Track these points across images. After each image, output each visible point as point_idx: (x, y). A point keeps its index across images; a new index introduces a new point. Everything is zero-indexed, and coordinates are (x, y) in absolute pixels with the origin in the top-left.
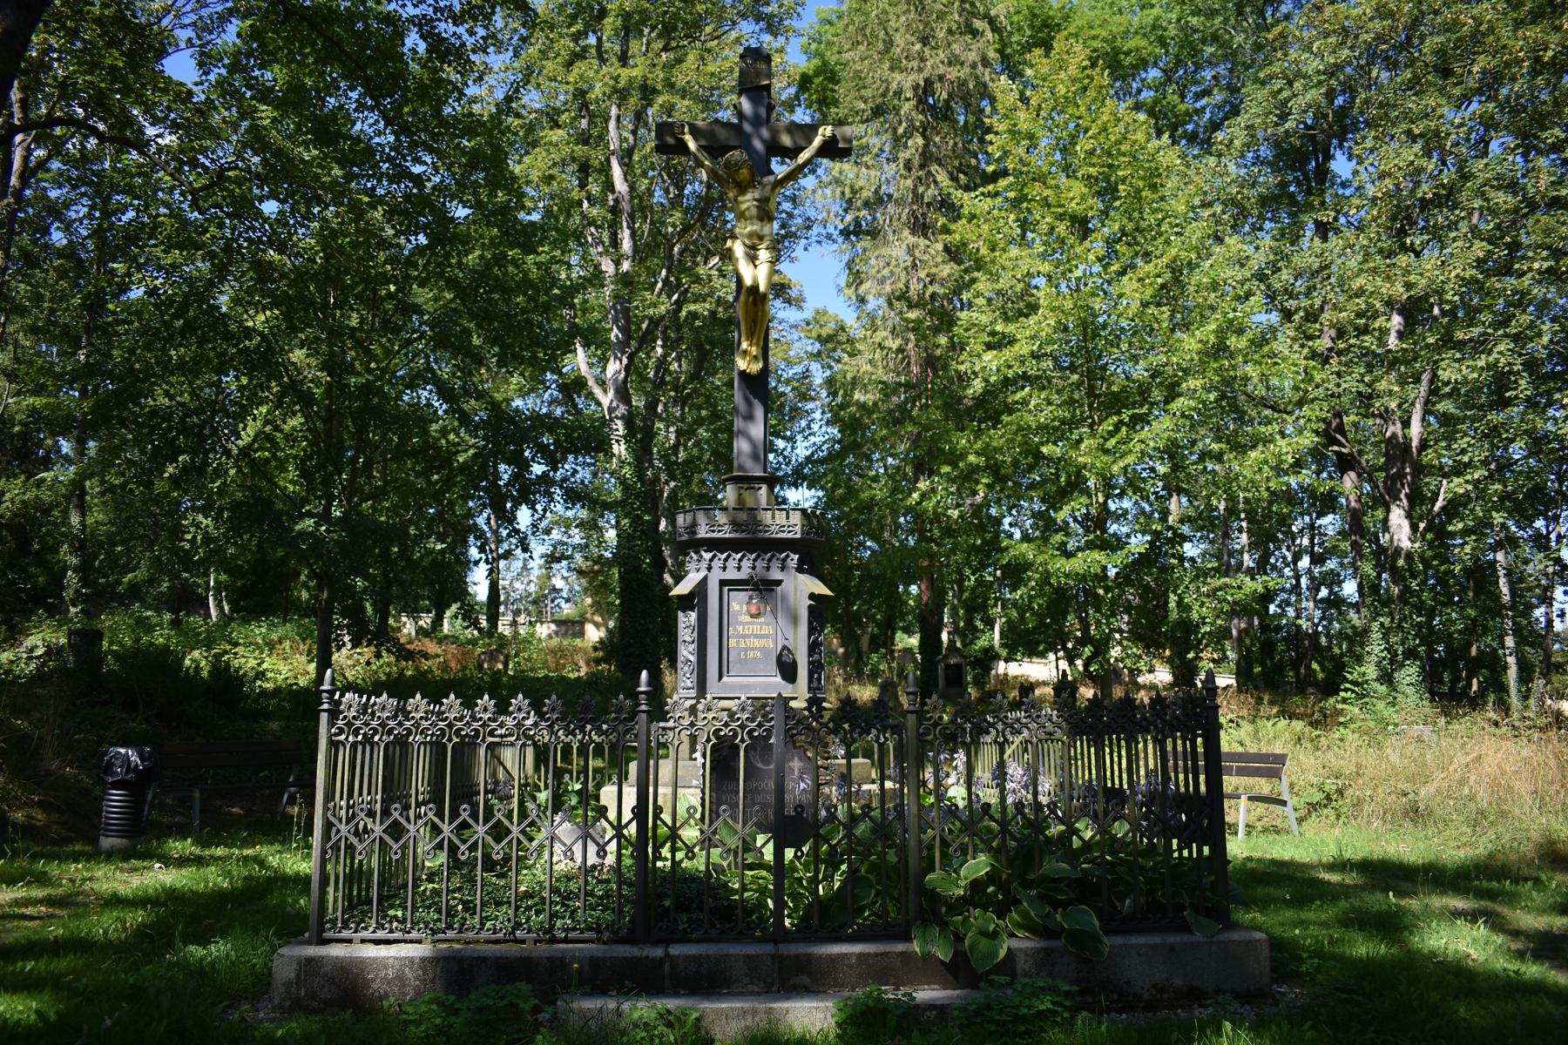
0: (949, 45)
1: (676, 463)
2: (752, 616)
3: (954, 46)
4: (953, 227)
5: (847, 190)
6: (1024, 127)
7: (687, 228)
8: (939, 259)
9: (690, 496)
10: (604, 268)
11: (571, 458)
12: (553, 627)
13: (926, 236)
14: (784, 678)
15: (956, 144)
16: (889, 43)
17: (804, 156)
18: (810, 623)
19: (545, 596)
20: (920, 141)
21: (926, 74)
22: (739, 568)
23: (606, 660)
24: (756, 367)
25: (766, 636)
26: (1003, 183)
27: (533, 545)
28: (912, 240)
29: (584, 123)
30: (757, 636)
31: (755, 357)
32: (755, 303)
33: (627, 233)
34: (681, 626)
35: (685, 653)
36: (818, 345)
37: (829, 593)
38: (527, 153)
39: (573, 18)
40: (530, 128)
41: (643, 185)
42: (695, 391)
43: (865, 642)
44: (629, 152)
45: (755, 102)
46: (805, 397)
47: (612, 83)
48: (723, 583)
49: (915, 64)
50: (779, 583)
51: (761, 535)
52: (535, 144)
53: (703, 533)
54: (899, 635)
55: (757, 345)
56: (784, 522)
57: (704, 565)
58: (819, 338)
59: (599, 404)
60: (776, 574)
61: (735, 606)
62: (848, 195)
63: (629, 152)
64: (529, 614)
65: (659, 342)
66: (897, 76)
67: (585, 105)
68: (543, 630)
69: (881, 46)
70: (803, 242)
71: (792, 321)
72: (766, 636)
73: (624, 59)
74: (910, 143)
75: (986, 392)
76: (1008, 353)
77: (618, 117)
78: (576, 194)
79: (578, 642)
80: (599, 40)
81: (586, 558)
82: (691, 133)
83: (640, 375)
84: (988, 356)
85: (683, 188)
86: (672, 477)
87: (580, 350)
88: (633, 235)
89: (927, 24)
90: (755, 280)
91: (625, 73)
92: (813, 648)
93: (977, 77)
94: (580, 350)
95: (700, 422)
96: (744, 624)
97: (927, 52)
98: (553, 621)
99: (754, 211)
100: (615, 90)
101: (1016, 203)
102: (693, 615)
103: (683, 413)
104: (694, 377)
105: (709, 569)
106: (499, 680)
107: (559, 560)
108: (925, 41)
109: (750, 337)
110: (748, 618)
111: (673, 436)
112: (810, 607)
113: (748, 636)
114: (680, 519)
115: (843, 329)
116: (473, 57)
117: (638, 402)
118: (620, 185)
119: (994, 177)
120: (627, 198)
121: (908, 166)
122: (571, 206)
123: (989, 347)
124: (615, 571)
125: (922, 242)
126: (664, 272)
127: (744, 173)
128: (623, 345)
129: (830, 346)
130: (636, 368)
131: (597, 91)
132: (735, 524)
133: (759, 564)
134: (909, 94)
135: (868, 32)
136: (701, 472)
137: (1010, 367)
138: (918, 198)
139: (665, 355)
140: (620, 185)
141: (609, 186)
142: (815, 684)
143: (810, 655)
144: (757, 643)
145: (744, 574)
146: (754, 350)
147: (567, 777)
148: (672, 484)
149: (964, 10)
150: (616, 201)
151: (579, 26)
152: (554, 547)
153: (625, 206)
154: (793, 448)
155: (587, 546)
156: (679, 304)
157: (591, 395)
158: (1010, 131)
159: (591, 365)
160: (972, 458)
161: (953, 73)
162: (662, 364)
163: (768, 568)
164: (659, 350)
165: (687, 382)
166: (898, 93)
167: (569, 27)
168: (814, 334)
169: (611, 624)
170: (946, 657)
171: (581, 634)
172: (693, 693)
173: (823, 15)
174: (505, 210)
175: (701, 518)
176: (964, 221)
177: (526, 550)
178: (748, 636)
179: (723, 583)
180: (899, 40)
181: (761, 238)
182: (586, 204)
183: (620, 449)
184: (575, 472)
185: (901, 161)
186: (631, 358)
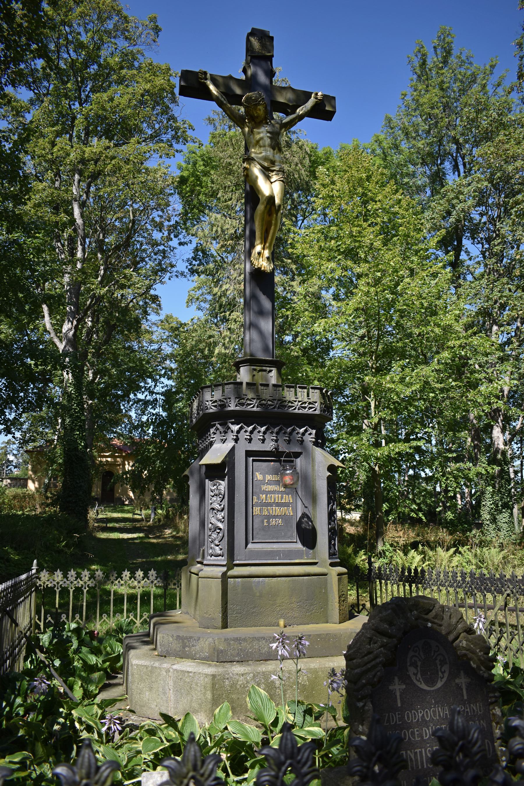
5: (219, 229)
12: (9, 481)
14: (304, 544)
17: (300, 111)
30: (278, 505)
32: (270, 214)
33: (80, 248)
35: (213, 520)
48: (249, 454)
56: (306, 400)
61: (259, 476)
70: (168, 274)
71: (153, 321)
99: (268, 141)
102: (223, 485)
105: (236, 440)
112: (329, 478)
120: (81, 227)
143: (329, 524)
144: (277, 511)
145: (269, 446)
147: (64, 617)
154: (155, 386)
171: (25, 486)
172: (223, 561)
186: (78, 321)
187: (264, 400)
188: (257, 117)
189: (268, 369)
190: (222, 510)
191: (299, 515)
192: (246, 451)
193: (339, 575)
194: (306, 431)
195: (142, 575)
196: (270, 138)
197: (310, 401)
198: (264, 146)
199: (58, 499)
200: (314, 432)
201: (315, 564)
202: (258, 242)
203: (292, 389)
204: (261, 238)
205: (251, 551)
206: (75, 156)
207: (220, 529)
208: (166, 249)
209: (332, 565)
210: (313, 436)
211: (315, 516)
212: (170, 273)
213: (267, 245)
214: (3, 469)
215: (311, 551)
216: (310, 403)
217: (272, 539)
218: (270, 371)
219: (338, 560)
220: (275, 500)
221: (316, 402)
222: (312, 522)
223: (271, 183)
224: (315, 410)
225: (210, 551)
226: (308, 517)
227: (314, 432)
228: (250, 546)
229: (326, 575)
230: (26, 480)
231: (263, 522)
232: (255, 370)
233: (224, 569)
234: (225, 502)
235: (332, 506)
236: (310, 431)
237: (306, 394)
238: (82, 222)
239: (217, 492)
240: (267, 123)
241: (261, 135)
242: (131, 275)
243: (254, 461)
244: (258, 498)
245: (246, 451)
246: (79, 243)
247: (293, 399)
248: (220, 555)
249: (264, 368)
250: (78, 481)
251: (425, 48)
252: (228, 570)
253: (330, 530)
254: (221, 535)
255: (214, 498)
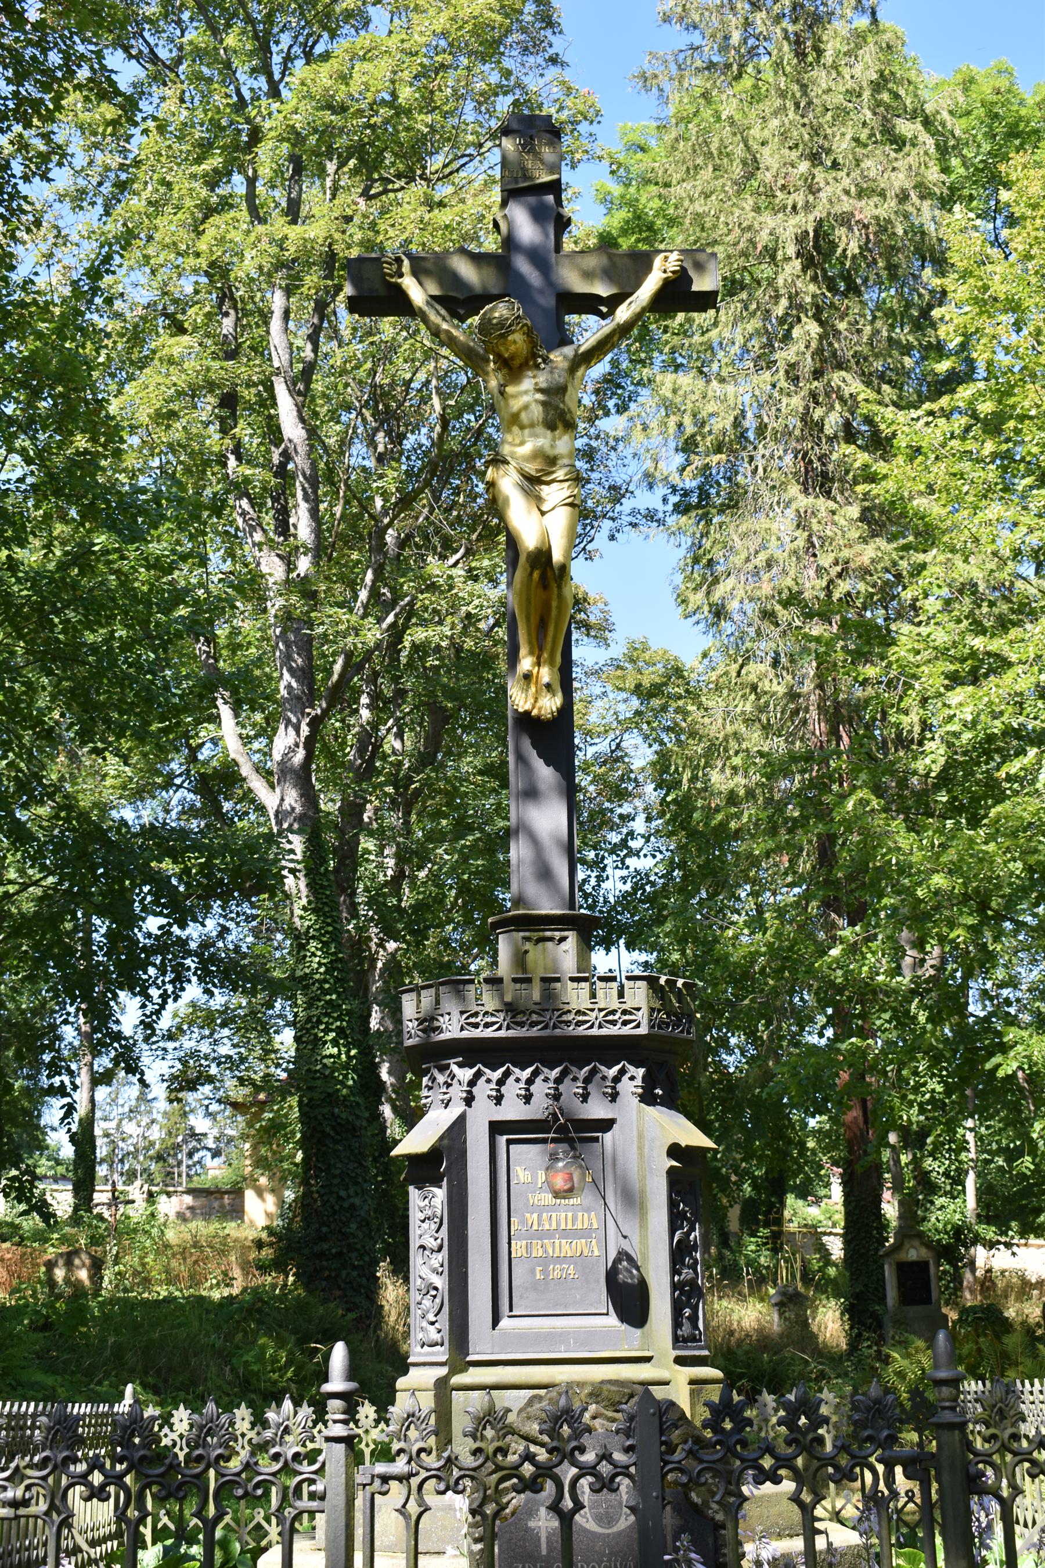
0: (858, 162)
1: (398, 908)
2: (557, 1195)
3: (867, 164)
4: (880, 467)
5: (687, 420)
6: (999, 289)
7: (406, 501)
8: (854, 534)
9: (423, 968)
10: (264, 569)
11: (216, 906)
12: (188, 1200)
13: (828, 495)
14: (623, 1317)
15: (876, 332)
16: (752, 166)
17: (623, 313)
18: (672, 1204)
19: (178, 1147)
20: (814, 328)
21: (819, 213)
22: (528, 1098)
23: (278, 1265)
24: (550, 704)
25: (585, 1234)
26: (965, 393)
27: (146, 1060)
28: (804, 502)
29: (228, 324)
30: (565, 1234)
31: (548, 686)
32: (544, 583)
33: (303, 507)
34: (415, 1216)
35: (425, 1271)
36: (635, 703)
37: (706, 1142)
38: (131, 378)
39: (205, 148)
40: (136, 336)
41: (331, 433)
42: (427, 783)
43: (734, 1224)
44: (309, 370)
45: (538, 215)
46: (621, 795)
47: (274, 250)
48: (496, 1128)
49: (799, 198)
50: (607, 1125)
51: (571, 1030)
52: (143, 364)
53: (451, 1028)
54: (790, 1199)
55: (551, 663)
56: (615, 1004)
57: (457, 1092)
58: (638, 690)
59: (261, 809)
60: (596, 1109)
61: (521, 1174)
62: (690, 429)
63: (309, 370)
64: (150, 1181)
65: (364, 700)
66: (769, 221)
67: (226, 295)
68: (168, 1206)
69: (737, 170)
70: (607, 525)
72: (585, 1234)
73: (293, 212)
74: (796, 332)
75: (950, 765)
76: (996, 688)
77: (286, 315)
78: (214, 441)
79: (231, 1228)
80: (251, 182)
81: (241, 1081)
82: (416, 273)
83: (331, 756)
84: (958, 695)
85: (402, 437)
86: (390, 933)
87: (225, 712)
88: (314, 513)
89: (816, 131)
90: (545, 536)
91: (295, 232)
92: (679, 1254)
93: (906, 216)
94: (225, 712)
95: (435, 837)
96: (541, 1209)
97: (820, 175)
98: (189, 1191)
99: (537, 412)
100: (280, 265)
101: (993, 426)
102: (439, 1195)
103: (407, 823)
104: (425, 759)
105: (469, 1100)
106: (84, 1309)
107: (192, 1086)
108: (815, 158)
109: (538, 651)
110: (548, 1198)
111: (391, 862)
112: (671, 1172)
113: (548, 1234)
114: (409, 1006)
115: (678, 672)
116: (24, 188)
117: (330, 804)
118: (292, 429)
119: (949, 383)
120: (302, 449)
121: (792, 373)
122: (207, 463)
123: (955, 680)
124: (294, 1101)
125: (823, 504)
126: (369, 576)
127: (518, 340)
128: (301, 701)
129: (656, 702)
130: (326, 747)
131: (247, 267)
132: (513, 1010)
133: (571, 1089)
134: (791, 250)
135: (714, 147)
136: (441, 926)
137: (996, 716)
138: (813, 427)
139: (375, 725)
140: (292, 429)
141: (273, 432)
142: (686, 1330)
143: (674, 1271)
144: (566, 1248)
145: (538, 1108)
146: (545, 674)
148: (391, 946)
149: (879, 103)
150: (286, 456)
151: (215, 161)
152: (185, 1063)
153: (300, 462)
154: (600, 879)
155: (243, 1060)
156: (396, 633)
157: (248, 796)
158: (976, 301)
159: (246, 740)
160: (939, 880)
161: (868, 210)
162: (369, 742)
163: (585, 1098)
164: (365, 714)
165: (415, 769)
166: (771, 254)
167: (198, 161)
168: (630, 684)
169: (289, 1195)
170: (897, 1248)
171: (237, 1212)
172: (441, 1354)
173: (631, 136)
174: (88, 462)
175: (450, 1005)
176: (900, 460)
177: (133, 1068)
178: (548, 1234)
179: (496, 1128)
180: (770, 158)
181: (552, 461)
182: (232, 462)
183: (296, 885)
184: (224, 931)
185: (782, 365)
186: (315, 723)
187: (523, 1012)
188: (512, 358)
189: (557, 935)
190: (440, 1249)
191: (612, 1255)
192: (492, 1124)
193: (692, 1382)
194: (623, 1072)
195: (373, 1416)
196: (544, 404)
197: (624, 1007)
198: (532, 425)
199: (288, 1249)
200: (641, 1071)
201: (648, 1359)
202: (523, 651)
203: (583, 984)
204: (530, 642)
205: (505, 1333)
206: (257, 261)
207: (436, 1289)
208: (594, 444)
209: (680, 1361)
210: (639, 1082)
211: (645, 1258)
212: (613, 519)
213: (546, 655)
214: (179, 1163)
215: (638, 1332)
216: (625, 1012)
217: (555, 1307)
218: (563, 939)
219: (706, 1353)
220: (558, 1224)
221: (638, 1009)
222: (638, 1268)
223: (543, 513)
224: (638, 1026)
225: (420, 1335)
226: (630, 1259)
227: (641, 1071)
228: (505, 1323)
229: (667, 1383)
230: (237, 1192)
231: (533, 1272)
232: (527, 939)
233: (443, 1371)
234: (444, 1232)
235: (688, 1234)
236: (632, 1070)
237: (615, 993)
238: (303, 434)
239: (429, 1213)
240: (537, 367)
241: (525, 399)
242: (450, 577)
243: (509, 1142)
244: (523, 1221)
245: (492, 1124)
246: (300, 494)
247: (585, 1004)
248: (436, 1344)
249: (548, 934)
250: (343, 1194)
251: (977, 70)
252: (453, 1372)
253: (674, 1287)
254: (438, 1300)
255: (425, 1225)
